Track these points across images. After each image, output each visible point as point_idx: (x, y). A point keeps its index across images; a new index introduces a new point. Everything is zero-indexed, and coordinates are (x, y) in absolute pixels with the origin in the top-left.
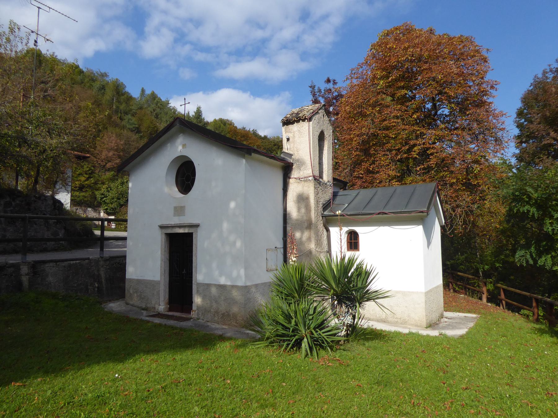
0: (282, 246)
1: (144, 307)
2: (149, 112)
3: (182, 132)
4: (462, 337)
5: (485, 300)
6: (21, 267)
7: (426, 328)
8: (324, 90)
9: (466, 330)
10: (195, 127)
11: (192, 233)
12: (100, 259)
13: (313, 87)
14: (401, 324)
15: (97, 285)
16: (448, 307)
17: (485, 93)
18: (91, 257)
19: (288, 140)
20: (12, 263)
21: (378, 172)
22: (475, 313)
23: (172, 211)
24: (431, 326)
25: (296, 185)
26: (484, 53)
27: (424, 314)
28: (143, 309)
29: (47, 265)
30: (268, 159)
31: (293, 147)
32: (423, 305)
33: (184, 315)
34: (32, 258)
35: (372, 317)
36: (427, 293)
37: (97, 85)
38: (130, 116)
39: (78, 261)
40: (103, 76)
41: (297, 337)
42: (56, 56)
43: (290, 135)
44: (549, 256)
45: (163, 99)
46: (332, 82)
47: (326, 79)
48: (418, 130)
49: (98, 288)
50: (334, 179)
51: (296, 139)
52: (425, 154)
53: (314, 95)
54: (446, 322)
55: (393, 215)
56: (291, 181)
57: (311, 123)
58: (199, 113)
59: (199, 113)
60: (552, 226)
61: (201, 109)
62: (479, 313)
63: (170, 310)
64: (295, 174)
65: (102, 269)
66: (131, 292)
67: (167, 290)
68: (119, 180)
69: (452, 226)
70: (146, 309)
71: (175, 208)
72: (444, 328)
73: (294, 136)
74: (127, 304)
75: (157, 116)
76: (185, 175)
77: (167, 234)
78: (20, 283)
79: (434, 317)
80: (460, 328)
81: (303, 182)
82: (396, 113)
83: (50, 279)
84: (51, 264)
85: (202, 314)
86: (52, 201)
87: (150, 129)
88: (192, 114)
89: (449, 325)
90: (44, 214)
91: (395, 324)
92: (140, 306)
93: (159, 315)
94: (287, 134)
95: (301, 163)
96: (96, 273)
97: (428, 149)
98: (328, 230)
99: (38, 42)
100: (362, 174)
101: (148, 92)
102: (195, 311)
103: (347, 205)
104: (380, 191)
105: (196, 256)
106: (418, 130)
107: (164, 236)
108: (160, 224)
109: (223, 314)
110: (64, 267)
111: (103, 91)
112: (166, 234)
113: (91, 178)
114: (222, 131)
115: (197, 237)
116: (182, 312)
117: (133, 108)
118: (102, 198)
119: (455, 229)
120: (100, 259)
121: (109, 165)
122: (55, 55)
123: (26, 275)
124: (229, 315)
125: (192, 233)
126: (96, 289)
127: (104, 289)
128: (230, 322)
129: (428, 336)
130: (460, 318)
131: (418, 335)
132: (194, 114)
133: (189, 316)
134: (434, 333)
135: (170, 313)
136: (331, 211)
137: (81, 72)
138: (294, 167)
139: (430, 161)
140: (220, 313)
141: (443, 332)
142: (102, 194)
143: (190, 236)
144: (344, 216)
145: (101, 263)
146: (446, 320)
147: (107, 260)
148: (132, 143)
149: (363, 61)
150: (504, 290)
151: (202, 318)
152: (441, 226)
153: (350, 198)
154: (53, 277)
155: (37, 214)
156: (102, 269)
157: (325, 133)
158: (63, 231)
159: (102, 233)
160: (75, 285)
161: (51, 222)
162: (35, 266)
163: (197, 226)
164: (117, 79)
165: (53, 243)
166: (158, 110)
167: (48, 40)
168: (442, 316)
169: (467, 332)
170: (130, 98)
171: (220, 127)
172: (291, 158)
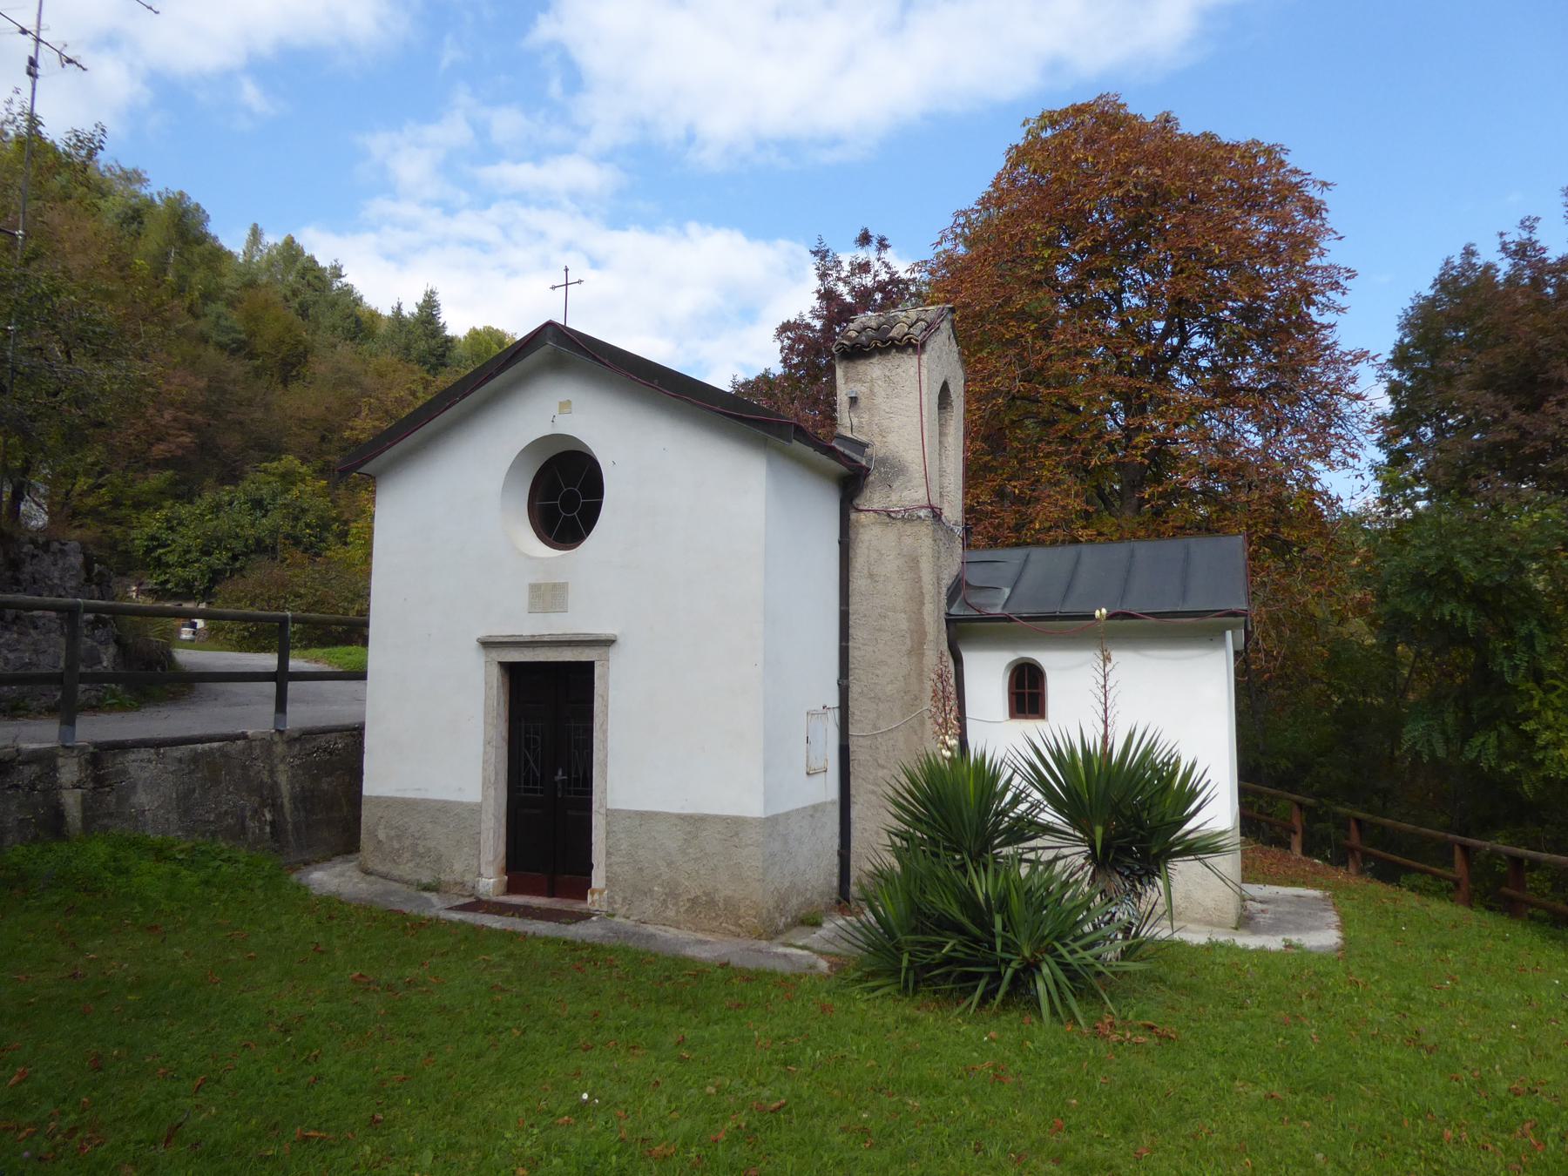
0: (836, 704)
2: (279, 299)
5: (1297, 850)
6: (60, 761)
8: (851, 263)
10: (562, 350)
11: (591, 665)
12: (276, 738)
15: (268, 817)
17: (1306, 293)
18: (250, 732)
19: (854, 401)
20: (34, 751)
22: (1315, 886)
23: (523, 599)
25: (877, 530)
26: (1313, 192)
28: (427, 888)
29: (132, 756)
31: (870, 424)
33: (578, 906)
34: (94, 729)
38: (220, 307)
39: (215, 745)
40: (128, 179)
43: (860, 389)
44: (1494, 735)
45: (324, 262)
46: (875, 242)
47: (857, 234)
49: (272, 824)
51: (878, 400)
55: (1152, 620)
57: (924, 357)
58: (429, 306)
59: (429, 306)
60: (1511, 658)
61: (437, 298)
62: (1326, 888)
63: (511, 888)
64: (874, 498)
65: (281, 767)
66: (382, 835)
67: (503, 831)
68: (208, 497)
71: (535, 589)
74: (367, 872)
75: (303, 311)
76: (565, 496)
77: (502, 665)
78: (58, 814)
81: (899, 524)
83: (142, 798)
84: (144, 754)
85: (624, 899)
86: (81, 558)
87: (284, 348)
92: (414, 877)
93: (478, 905)
95: (894, 470)
96: (265, 777)
98: (958, 662)
99: (40, 62)
101: (272, 239)
102: (601, 892)
103: (1007, 591)
104: (1037, 554)
105: (605, 732)
107: (495, 671)
108: (483, 633)
109: (694, 901)
110: (180, 760)
111: (135, 226)
112: (502, 665)
113: (101, 486)
115: (605, 676)
116: (553, 896)
117: (226, 281)
118: (149, 550)
121: (159, 450)
123: (75, 787)
124: (712, 903)
125: (591, 665)
126: (268, 829)
127: (290, 827)
128: (715, 924)
132: (416, 310)
133: (578, 906)
138: (871, 478)
141: (1294, 938)
142: (153, 538)
143: (585, 671)
144: (1011, 620)
145: (280, 749)
147: (296, 740)
148: (230, 388)
150: (1358, 821)
151: (623, 911)
156: (281, 767)
158: (112, 650)
159: (283, 661)
162: (100, 757)
163: (607, 643)
164: (182, 194)
166: (309, 295)
167: (70, 61)
170: (218, 255)
172: (862, 453)
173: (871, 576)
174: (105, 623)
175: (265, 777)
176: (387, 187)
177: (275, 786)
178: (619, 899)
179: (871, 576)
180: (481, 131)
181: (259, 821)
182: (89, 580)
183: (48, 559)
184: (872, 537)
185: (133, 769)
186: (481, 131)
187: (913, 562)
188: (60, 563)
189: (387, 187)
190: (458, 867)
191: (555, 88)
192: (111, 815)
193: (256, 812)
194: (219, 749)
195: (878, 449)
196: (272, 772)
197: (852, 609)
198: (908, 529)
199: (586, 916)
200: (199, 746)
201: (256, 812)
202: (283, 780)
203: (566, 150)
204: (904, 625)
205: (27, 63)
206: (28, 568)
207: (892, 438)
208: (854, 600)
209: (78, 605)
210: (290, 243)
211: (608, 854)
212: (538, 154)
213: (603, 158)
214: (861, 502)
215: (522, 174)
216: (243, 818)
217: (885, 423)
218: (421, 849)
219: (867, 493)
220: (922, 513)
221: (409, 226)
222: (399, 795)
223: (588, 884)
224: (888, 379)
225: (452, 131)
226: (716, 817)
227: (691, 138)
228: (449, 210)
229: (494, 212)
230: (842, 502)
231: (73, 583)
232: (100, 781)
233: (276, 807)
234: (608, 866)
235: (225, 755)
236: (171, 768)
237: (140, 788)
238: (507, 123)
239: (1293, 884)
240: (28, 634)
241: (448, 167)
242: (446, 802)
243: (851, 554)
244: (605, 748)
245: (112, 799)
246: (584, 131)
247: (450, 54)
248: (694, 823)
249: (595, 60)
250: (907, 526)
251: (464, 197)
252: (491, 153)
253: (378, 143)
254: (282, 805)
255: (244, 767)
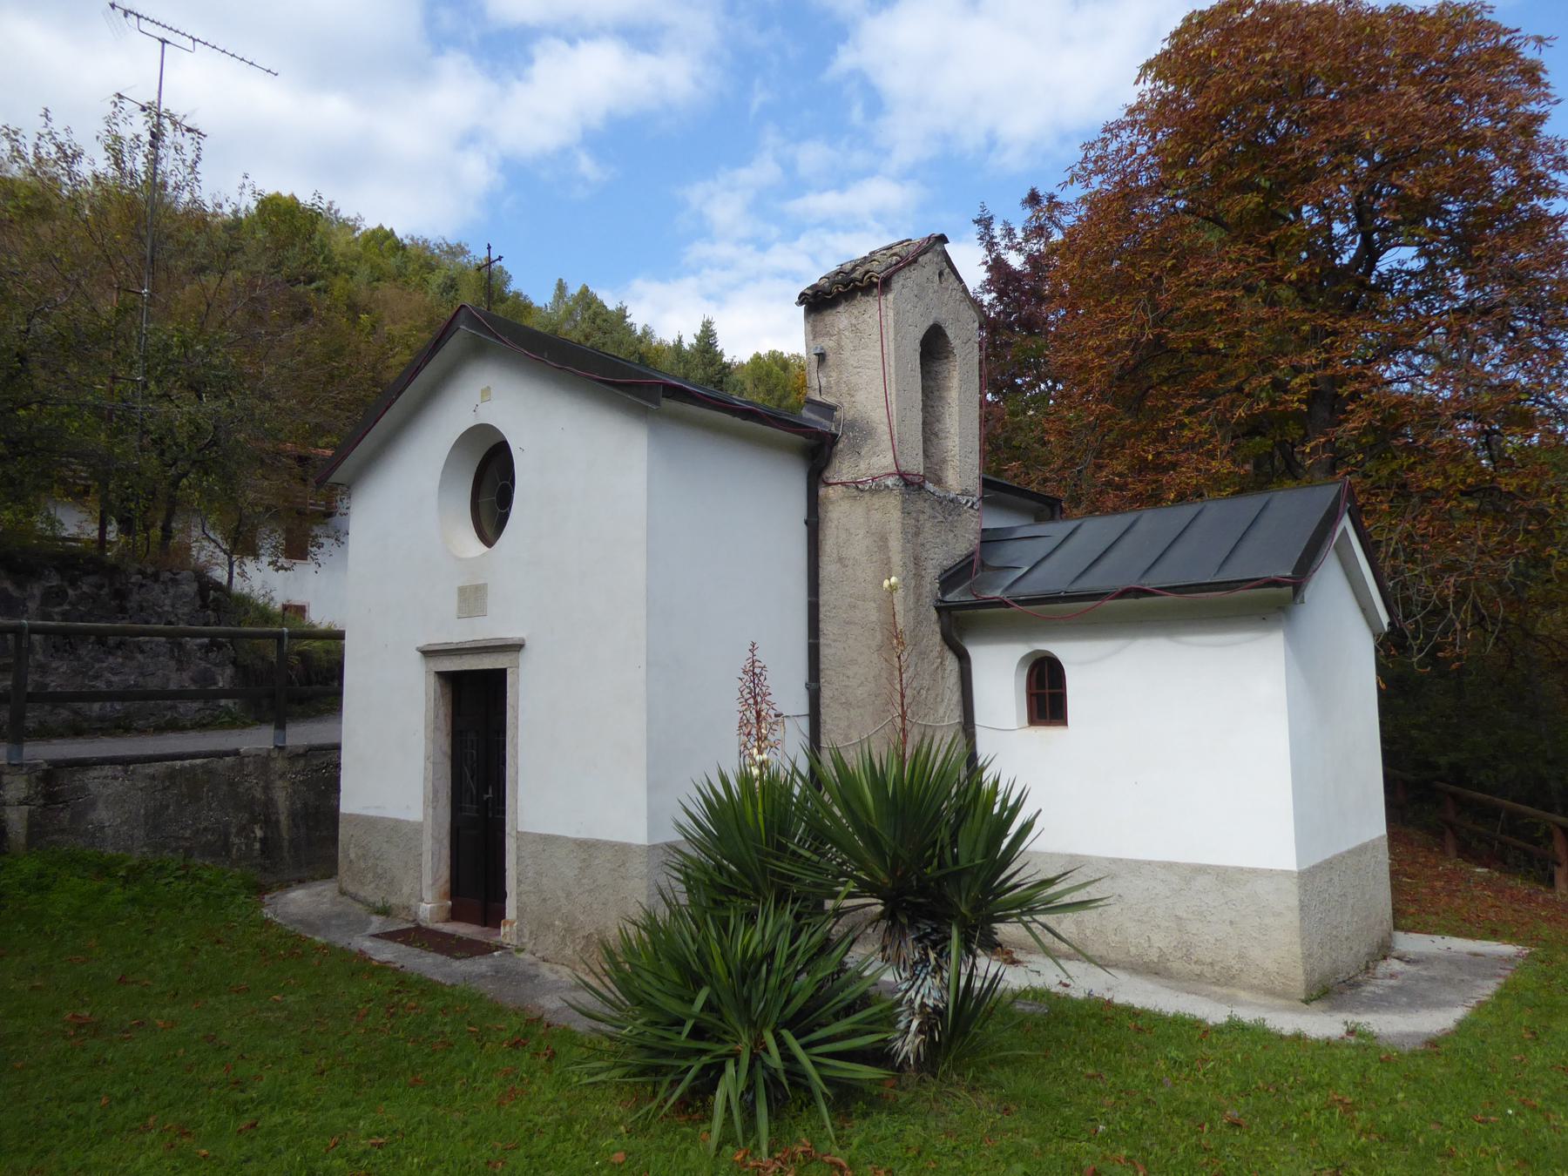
1: (380, 904)
3: (478, 351)
4: (1434, 1045)
6: (6, 779)
7: (1306, 1002)
8: (1024, 229)
9: (1459, 1013)
13: (985, 223)
14: (1217, 983)
15: (259, 833)
16: (1410, 910)
21: (1174, 466)
22: (1513, 938)
23: (452, 603)
24: (1326, 991)
25: (845, 506)
26: (1528, 53)
27: (1298, 950)
29: (93, 773)
30: (737, 420)
32: (1293, 917)
34: (42, 752)
35: (1113, 956)
36: (1308, 877)
37: (437, 279)
39: (198, 761)
41: (705, 1059)
42: (337, 211)
45: (611, 305)
47: (1025, 195)
48: (1304, 321)
49: (263, 841)
50: (986, 484)
51: (846, 354)
52: (1328, 401)
53: (991, 246)
54: (1392, 976)
55: (1171, 598)
56: (829, 493)
58: (707, 336)
59: (707, 336)
61: (714, 327)
63: (455, 915)
64: (843, 469)
65: (279, 783)
66: (352, 856)
69: (1429, 637)
70: (385, 911)
71: (462, 591)
72: (1377, 1003)
73: (840, 347)
76: (491, 480)
77: (441, 675)
79: (1348, 955)
80: (1439, 1005)
81: (867, 495)
82: (1226, 270)
83: (102, 814)
84: (108, 770)
86: (195, 586)
88: (689, 341)
89: (1399, 990)
90: (170, 623)
91: (1192, 982)
93: (417, 936)
94: (820, 340)
95: (862, 431)
97: (1342, 380)
98: (964, 659)
100: (1120, 475)
101: (574, 290)
106: (1304, 321)
107: (432, 679)
110: (153, 777)
114: (776, 385)
119: (1438, 647)
120: (275, 755)
122: (335, 207)
123: (21, 803)
126: (257, 846)
127: (286, 844)
129: (1298, 1038)
130: (1453, 961)
131: (1259, 1035)
132: (253, 205)
133: (493, 940)
134: (1323, 1025)
135: (449, 928)
136: (970, 590)
137: (399, 247)
138: (840, 446)
139: (1347, 420)
140: (581, 933)
144: (1007, 605)
146: (1396, 966)
147: (298, 756)
149: (1121, 115)
152: (1376, 636)
153: (1042, 548)
154: (112, 808)
155: (147, 622)
157: (950, 333)
158: (229, 671)
160: (188, 833)
161: (192, 643)
163: (516, 647)
165: (196, 705)
168: (1384, 951)
169: (1460, 1023)
171: (769, 374)
172: (830, 418)
173: (840, 560)
174: (220, 646)
175: (258, 794)
176: (703, 231)
177: (270, 803)
178: (526, 932)
179: (840, 560)
180: (789, 167)
181: (247, 837)
182: (204, 606)
183: (157, 588)
184: (841, 513)
185: (93, 786)
186: (789, 167)
187: (882, 541)
188: (171, 591)
189: (703, 231)
190: (406, 890)
191: (857, 115)
192: (63, 831)
193: (244, 830)
194: (202, 766)
195: (846, 413)
196: (267, 788)
197: (823, 599)
198: (877, 501)
199: (483, 949)
200: (178, 763)
201: (244, 830)
202: (281, 797)
203: (870, 173)
204: (874, 616)
205: (938, 233)
206: (135, 598)
207: (861, 397)
208: (824, 588)
209: (22, 627)
210: (585, 292)
211: (519, 882)
212: (841, 180)
213: (906, 176)
214: (832, 475)
215: (828, 202)
216: (227, 835)
217: (853, 379)
218: (380, 871)
219: (836, 463)
220: (890, 482)
221: (726, 266)
222: (364, 812)
223: (503, 916)
224: (855, 329)
225: (764, 171)
226: (606, 843)
227: (992, 143)
228: (762, 245)
229: (803, 242)
230: (809, 477)
231: (186, 610)
232: (51, 798)
233: (270, 823)
234: (519, 895)
235: (210, 772)
236: (141, 785)
237: (100, 805)
238: (812, 156)
239: (1472, 937)
240: (133, 659)
241: (759, 206)
242: (398, 821)
243: (821, 537)
244: (516, 765)
245: (65, 816)
246: (886, 153)
247: (759, 98)
248: (588, 847)
249: (895, 82)
250: (875, 499)
251: (774, 231)
252: (795, 186)
253: (695, 193)
254: (278, 821)
255: (232, 784)
